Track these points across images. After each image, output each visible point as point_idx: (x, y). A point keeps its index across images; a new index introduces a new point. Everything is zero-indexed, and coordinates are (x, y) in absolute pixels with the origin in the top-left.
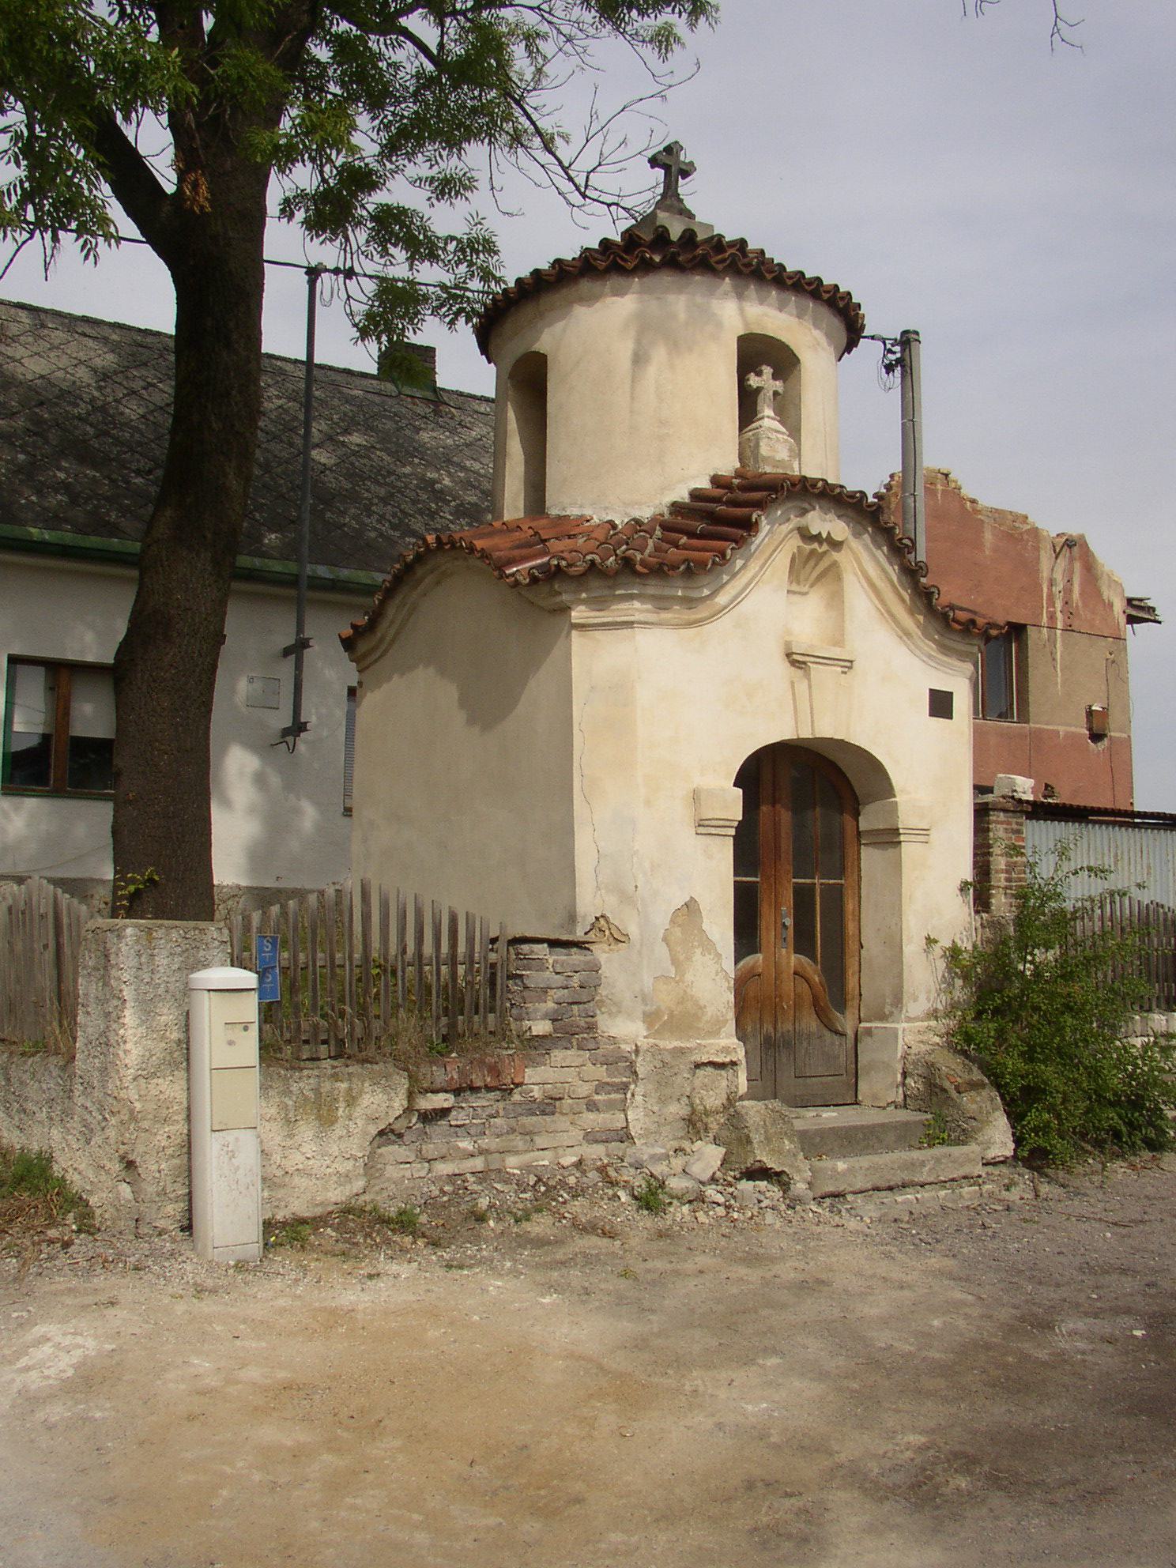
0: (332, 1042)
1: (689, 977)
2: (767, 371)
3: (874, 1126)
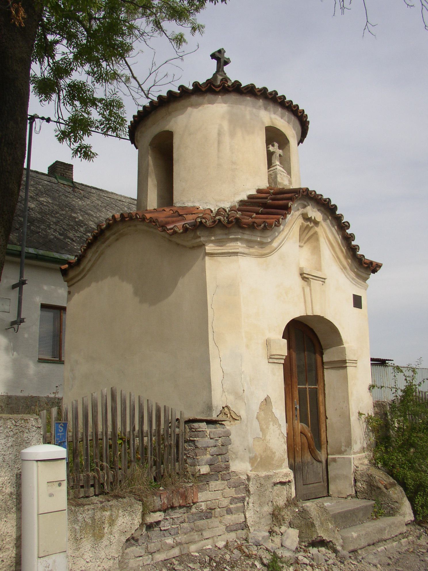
0: (97, 486)
1: (268, 437)
2: (276, 145)
3: (354, 510)
